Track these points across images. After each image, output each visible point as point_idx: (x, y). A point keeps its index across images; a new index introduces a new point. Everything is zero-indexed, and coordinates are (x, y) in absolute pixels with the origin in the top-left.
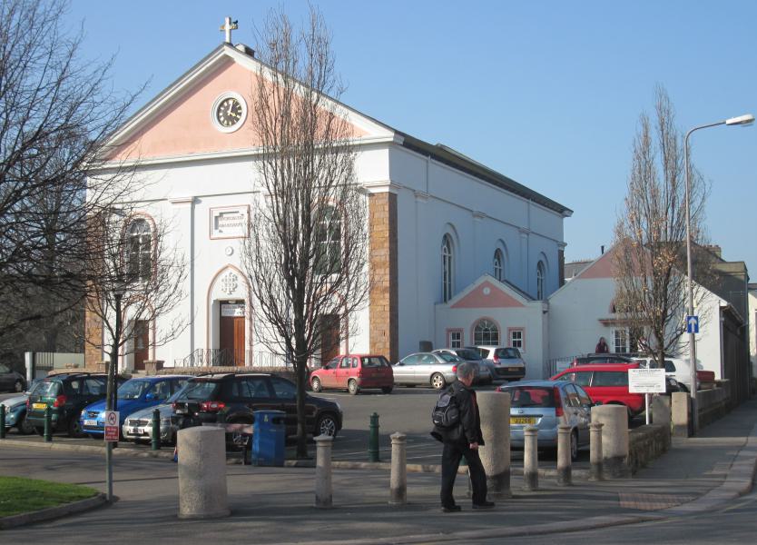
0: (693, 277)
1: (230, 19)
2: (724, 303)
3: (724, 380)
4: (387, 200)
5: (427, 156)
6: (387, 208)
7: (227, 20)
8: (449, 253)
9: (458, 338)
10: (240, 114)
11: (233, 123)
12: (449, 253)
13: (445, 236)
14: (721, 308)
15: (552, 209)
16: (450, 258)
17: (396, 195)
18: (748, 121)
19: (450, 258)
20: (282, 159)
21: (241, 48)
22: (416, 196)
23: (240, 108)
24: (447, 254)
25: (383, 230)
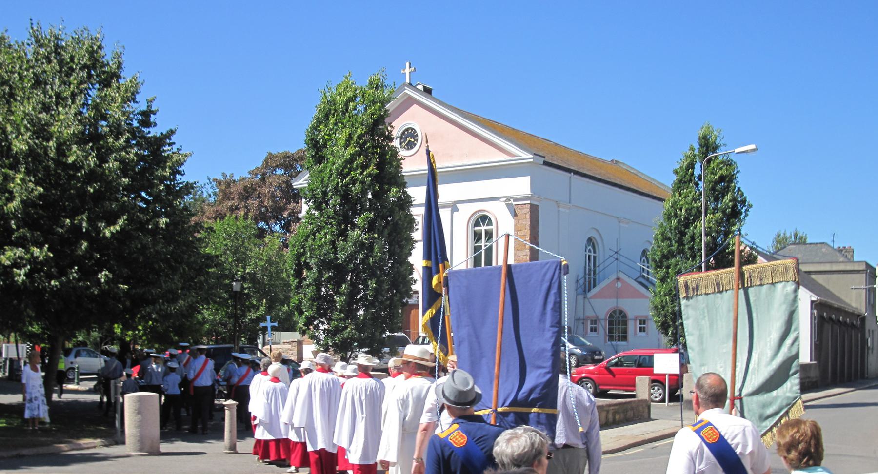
0: (474, 257)
1: (410, 64)
2: (815, 298)
3: (813, 362)
4: (528, 210)
5: (570, 173)
6: (528, 216)
7: (407, 64)
8: (595, 252)
9: (644, 323)
10: (417, 140)
11: (412, 148)
12: (595, 252)
13: (590, 240)
14: (812, 302)
15: (514, 129)
16: (595, 257)
17: (538, 206)
18: (754, 150)
19: (595, 257)
20: (359, 154)
21: (420, 87)
22: (620, 222)
23: (417, 136)
24: (592, 254)
25: (817, 265)
